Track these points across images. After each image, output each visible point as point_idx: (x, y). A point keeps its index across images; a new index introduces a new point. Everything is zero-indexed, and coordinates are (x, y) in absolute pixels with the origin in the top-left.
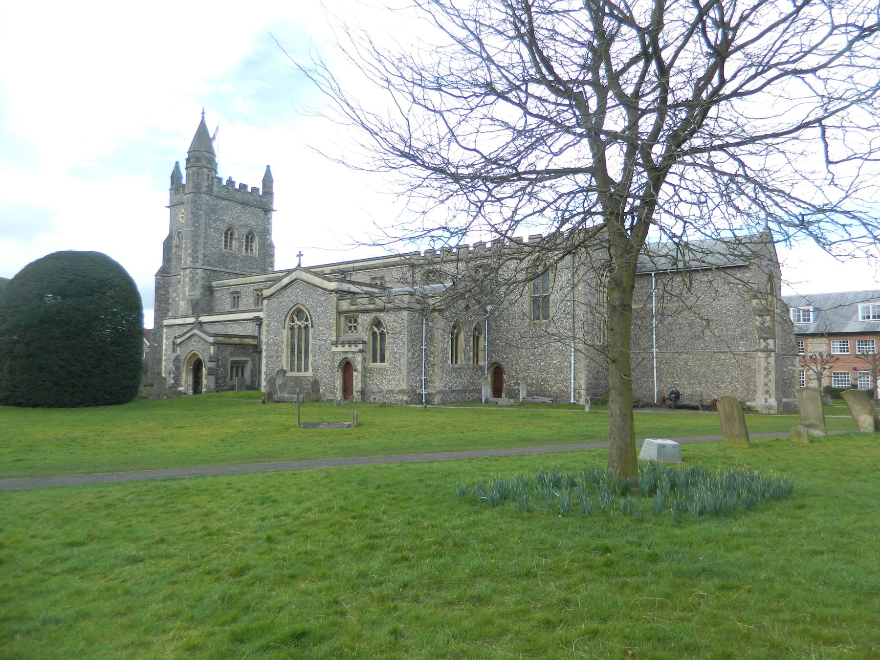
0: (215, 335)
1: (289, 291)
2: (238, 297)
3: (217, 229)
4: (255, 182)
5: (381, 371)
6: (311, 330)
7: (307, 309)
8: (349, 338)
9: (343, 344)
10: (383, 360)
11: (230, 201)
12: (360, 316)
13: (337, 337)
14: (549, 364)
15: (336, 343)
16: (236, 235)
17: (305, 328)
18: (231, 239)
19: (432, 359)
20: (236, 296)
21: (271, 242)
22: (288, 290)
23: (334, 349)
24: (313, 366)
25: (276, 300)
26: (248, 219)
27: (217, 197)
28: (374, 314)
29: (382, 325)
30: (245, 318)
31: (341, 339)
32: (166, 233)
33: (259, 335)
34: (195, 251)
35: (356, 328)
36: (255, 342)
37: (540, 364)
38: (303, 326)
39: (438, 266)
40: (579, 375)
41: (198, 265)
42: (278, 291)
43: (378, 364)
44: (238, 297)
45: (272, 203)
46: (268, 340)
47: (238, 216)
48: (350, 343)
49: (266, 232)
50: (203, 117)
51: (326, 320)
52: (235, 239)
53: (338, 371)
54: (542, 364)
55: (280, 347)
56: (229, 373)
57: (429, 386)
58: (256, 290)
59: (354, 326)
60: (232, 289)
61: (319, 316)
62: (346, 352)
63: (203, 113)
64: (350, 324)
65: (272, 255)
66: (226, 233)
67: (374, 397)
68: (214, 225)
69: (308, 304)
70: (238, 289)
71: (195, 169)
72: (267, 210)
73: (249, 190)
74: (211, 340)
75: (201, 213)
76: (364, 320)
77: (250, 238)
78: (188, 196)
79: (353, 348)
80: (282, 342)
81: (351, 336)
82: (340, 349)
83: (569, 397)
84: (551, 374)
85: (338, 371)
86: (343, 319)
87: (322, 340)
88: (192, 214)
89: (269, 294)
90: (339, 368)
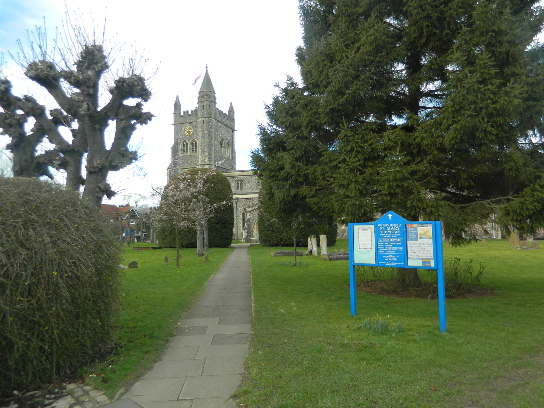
20: (239, 182)
26: (223, 132)
32: (172, 142)
34: (210, 154)
41: (212, 163)
50: (207, 70)
52: (223, 147)
60: (236, 178)
63: (207, 68)
71: (208, 102)
75: (212, 130)
88: (207, 130)
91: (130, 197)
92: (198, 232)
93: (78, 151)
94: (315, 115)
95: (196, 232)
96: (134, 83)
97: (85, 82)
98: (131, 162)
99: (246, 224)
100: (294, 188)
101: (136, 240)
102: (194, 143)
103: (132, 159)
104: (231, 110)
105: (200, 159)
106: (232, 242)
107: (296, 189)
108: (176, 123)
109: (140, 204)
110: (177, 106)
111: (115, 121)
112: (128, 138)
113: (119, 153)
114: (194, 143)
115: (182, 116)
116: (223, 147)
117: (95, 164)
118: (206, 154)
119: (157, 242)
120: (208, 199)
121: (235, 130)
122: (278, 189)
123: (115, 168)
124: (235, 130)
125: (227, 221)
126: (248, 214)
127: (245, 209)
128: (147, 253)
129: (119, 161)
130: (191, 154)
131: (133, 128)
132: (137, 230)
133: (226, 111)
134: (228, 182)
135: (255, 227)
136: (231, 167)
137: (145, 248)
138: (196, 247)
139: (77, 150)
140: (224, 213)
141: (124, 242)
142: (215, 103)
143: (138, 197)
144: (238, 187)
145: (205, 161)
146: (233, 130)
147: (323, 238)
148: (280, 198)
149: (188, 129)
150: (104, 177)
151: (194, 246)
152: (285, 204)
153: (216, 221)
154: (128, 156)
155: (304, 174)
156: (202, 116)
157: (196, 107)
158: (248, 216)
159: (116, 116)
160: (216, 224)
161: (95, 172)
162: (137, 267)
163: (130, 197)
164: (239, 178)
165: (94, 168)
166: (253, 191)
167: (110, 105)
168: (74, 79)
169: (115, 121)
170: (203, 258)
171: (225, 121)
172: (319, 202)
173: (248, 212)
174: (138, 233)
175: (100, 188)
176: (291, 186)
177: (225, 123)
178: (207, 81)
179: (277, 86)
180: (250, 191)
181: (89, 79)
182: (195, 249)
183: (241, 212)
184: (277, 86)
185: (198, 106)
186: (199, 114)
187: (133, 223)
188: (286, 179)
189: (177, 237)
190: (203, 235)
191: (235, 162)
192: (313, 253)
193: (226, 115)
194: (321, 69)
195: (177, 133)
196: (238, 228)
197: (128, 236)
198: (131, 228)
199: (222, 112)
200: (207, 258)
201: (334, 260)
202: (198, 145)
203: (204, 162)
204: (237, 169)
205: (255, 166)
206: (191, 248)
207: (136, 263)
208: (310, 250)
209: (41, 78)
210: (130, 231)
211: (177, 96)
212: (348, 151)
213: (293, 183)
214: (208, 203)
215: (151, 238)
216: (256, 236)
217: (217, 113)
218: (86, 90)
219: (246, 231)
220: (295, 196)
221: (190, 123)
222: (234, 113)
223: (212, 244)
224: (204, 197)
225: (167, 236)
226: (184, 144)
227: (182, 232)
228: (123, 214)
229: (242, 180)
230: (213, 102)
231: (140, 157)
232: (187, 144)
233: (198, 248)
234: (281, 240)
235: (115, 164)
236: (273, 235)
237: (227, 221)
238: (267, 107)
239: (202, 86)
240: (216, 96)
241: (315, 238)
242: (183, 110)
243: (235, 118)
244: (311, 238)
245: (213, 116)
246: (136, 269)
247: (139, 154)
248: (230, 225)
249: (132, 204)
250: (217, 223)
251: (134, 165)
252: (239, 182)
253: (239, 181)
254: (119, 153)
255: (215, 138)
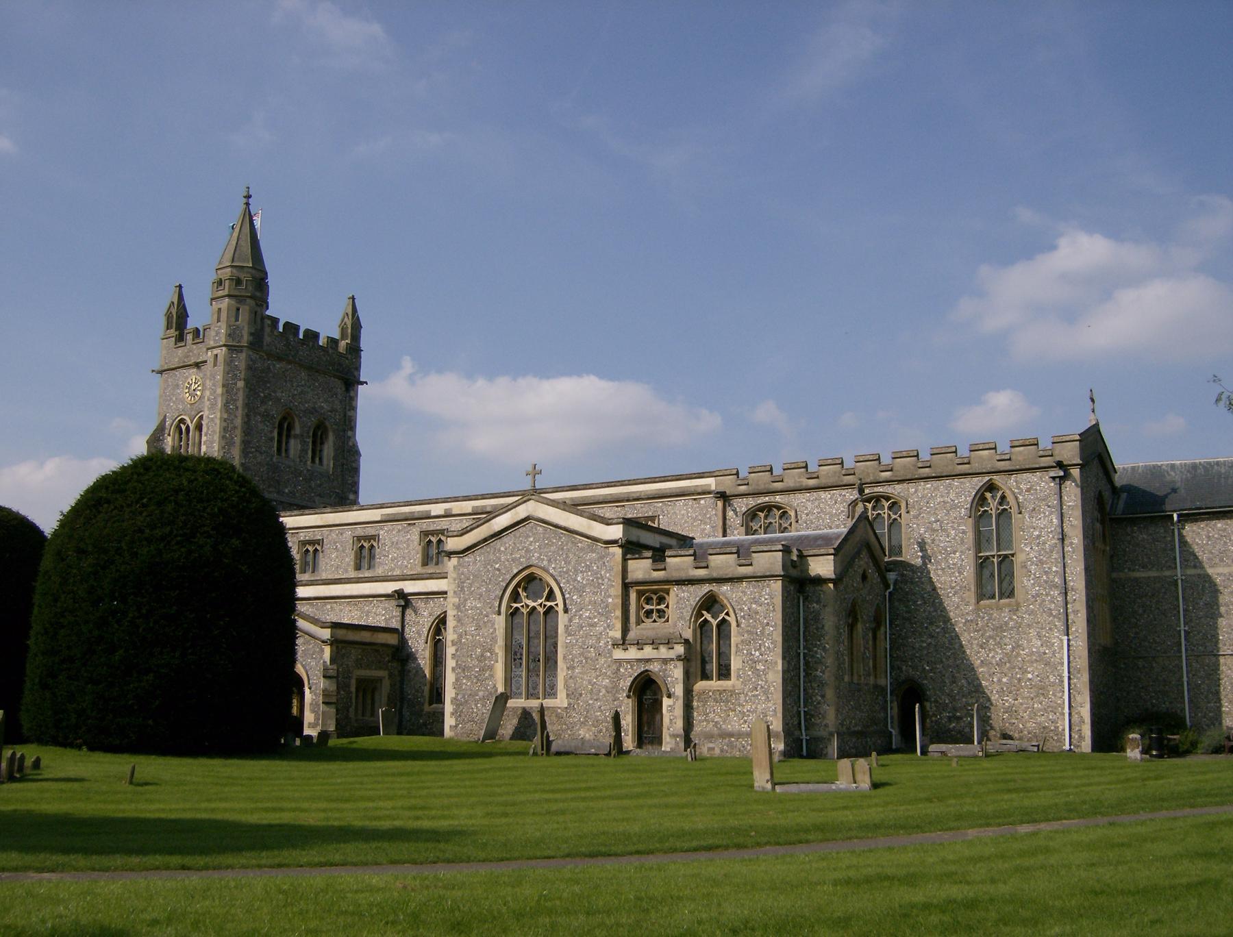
0: (335, 626)
1: (508, 541)
2: (316, 550)
3: (266, 416)
4: (328, 327)
5: (723, 697)
6: (562, 619)
7: (552, 575)
8: (651, 634)
9: (639, 645)
10: (724, 673)
11: (290, 362)
12: (675, 590)
13: (625, 630)
14: (1019, 680)
15: (623, 643)
16: (297, 430)
17: (546, 613)
18: (288, 436)
19: (818, 673)
20: (311, 549)
21: (355, 446)
22: (505, 539)
23: (619, 654)
24: (567, 687)
25: (478, 557)
27: (270, 355)
28: (706, 588)
29: (723, 607)
30: (367, 592)
31: (632, 635)
33: (403, 626)
35: (661, 613)
36: (392, 640)
37: (1000, 681)
38: (541, 610)
39: (778, 498)
40: (1079, 698)
42: (485, 540)
43: (714, 684)
44: (316, 550)
45: (358, 368)
46: (460, 636)
47: (302, 392)
48: (655, 643)
49: (348, 424)
50: (248, 204)
51: (598, 598)
53: (628, 697)
54: (1004, 680)
55: (491, 651)
56: (354, 701)
57: (814, 724)
58: (359, 538)
59: (658, 611)
61: (580, 590)
62: (648, 661)
64: (648, 607)
65: (356, 471)
66: (280, 426)
67: (711, 745)
68: (262, 409)
69: (552, 570)
70: (370, 531)
72: (350, 381)
73: (322, 341)
74: (326, 634)
76: (681, 602)
77: (318, 435)
78: (215, 351)
79: (664, 652)
80: (494, 640)
81: (649, 628)
82: (632, 653)
83: (1060, 741)
84: (1023, 698)
85: (628, 697)
86: (633, 596)
87: (587, 636)
89: (462, 547)
90: (630, 691)
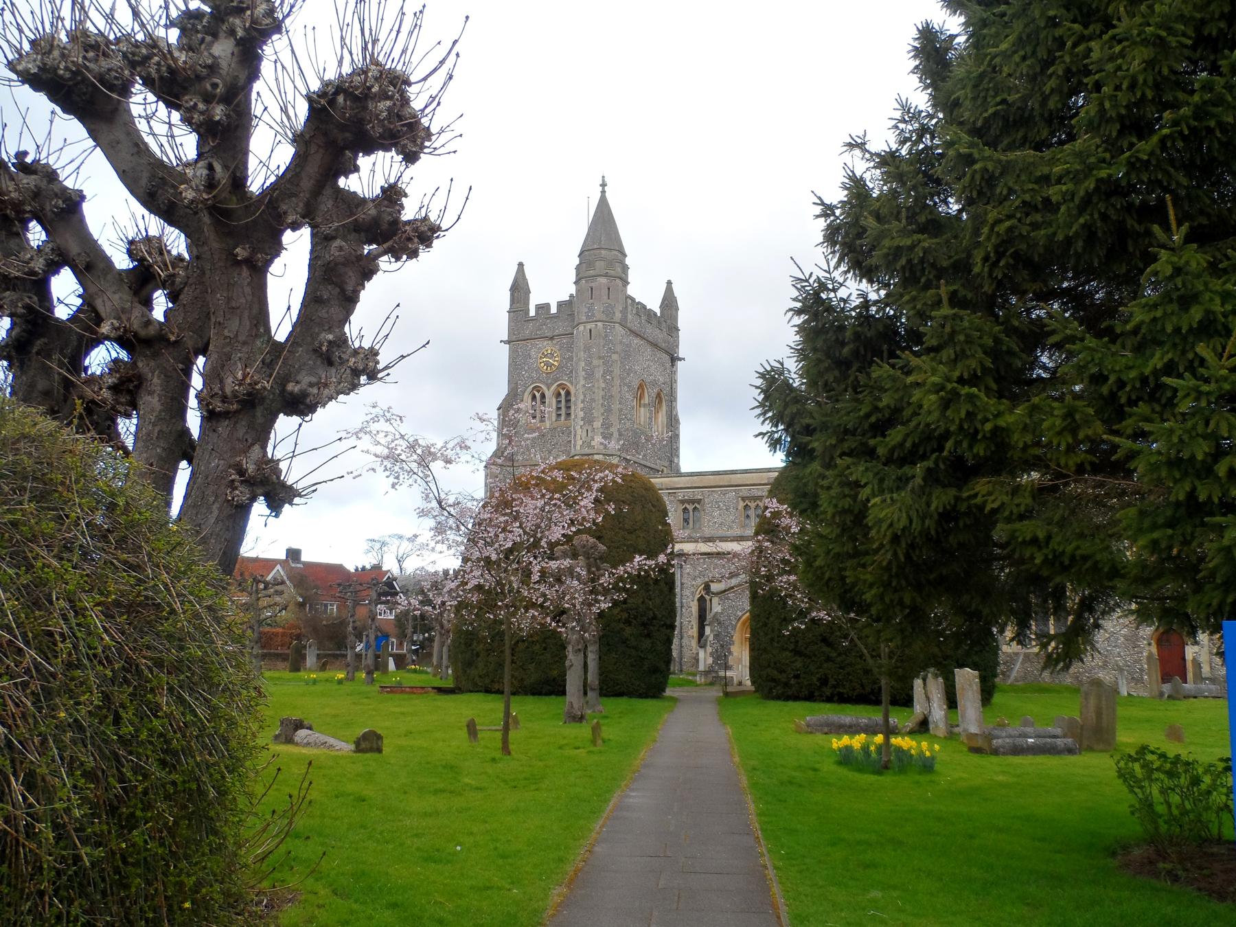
20: (690, 507)
26: (647, 364)
34: (606, 425)
50: (603, 192)
63: (603, 185)
91: (384, 544)
92: (570, 648)
93: (176, 342)
94: (1027, 215)
95: (565, 648)
96: (369, 88)
97: (199, 78)
98: (354, 386)
99: (708, 630)
100: (944, 486)
101: (392, 665)
102: (563, 393)
103: (356, 373)
104: (669, 301)
105: (578, 437)
106: (669, 682)
107: (952, 492)
108: (514, 338)
109: (411, 566)
110: (519, 289)
111: (306, 232)
112: (349, 301)
113: (315, 351)
114: (563, 393)
115: (532, 319)
116: (645, 405)
117: (230, 386)
118: (597, 424)
119: (450, 671)
120: (602, 547)
121: (680, 359)
122: (882, 492)
123: (301, 406)
124: (680, 359)
125: (654, 618)
126: (715, 600)
127: (707, 587)
128: (420, 704)
129: (314, 380)
130: (555, 425)
131: (368, 271)
132: (397, 637)
133: (654, 305)
134: (659, 500)
135: (737, 637)
136: (666, 464)
137: (414, 690)
138: (563, 693)
139: (173, 338)
140: (648, 591)
141: (357, 669)
142: (626, 283)
143: (406, 546)
144: (686, 521)
145: (593, 443)
146: (674, 359)
147: (966, 678)
148: (891, 525)
149: (546, 355)
150: (262, 434)
151: (557, 688)
152: (912, 546)
153: (625, 615)
154: (343, 362)
155: (996, 429)
156: (587, 316)
157: (571, 296)
158: (716, 607)
159: (309, 216)
160: (622, 625)
161: (226, 415)
162: (379, 750)
163: (384, 544)
164: (689, 494)
165: (224, 399)
166: (729, 533)
167: (288, 176)
168: (158, 64)
169: (306, 232)
170: (584, 731)
171: (651, 331)
172: (1049, 538)
173: (716, 594)
174: (400, 645)
175: (241, 472)
176: (931, 477)
177: (650, 339)
178: (603, 221)
179: (856, 145)
180: (720, 533)
181: (213, 68)
182: (560, 699)
183: (693, 594)
184: (856, 145)
185: (577, 291)
186: (582, 313)
187: (386, 615)
188: (909, 457)
189: (508, 661)
190: (585, 657)
191: (678, 449)
192: (931, 726)
193: (655, 314)
194: (1042, 53)
195: (516, 366)
196: (685, 641)
197: (370, 653)
198: (378, 629)
199: (644, 307)
200: (596, 729)
201: (1004, 754)
202: (573, 399)
203: (590, 446)
204: (685, 468)
205: (775, 421)
206: (546, 694)
207: (379, 737)
208: (921, 717)
209: (61, 77)
210: (377, 637)
211: (521, 265)
212: (1191, 329)
213: (942, 466)
214: (601, 558)
215: (435, 660)
216: (740, 669)
217: (630, 308)
218: (201, 106)
219: (709, 649)
220: (948, 516)
221: (552, 338)
222: (677, 309)
223: (611, 688)
224: (592, 540)
225: (478, 655)
226: (534, 397)
227: (521, 646)
228: (359, 588)
229: (699, 501)
230: (621, 278)
231: (387, 368)
232: (543, 396)
233: (568, 698)
234: (824, 681)
235: (297, 389)
236: (798, 664)
237: (654, 618)
238: (828, 210)
239: (588, 234)
240: (628, 261)
241: (941, 680)
242: (535, 300)
243: (680, 325)
244: (924, 680)
245: (618, 316)
246: (376, 755)
247: (383, 360)
248: (663, 629)
249: (390, 565)
250: (628, 622)
251: (367, 393)
252: (690, 507)
253: (692, 502)
254: (315, 351)
255: (622, 379)
